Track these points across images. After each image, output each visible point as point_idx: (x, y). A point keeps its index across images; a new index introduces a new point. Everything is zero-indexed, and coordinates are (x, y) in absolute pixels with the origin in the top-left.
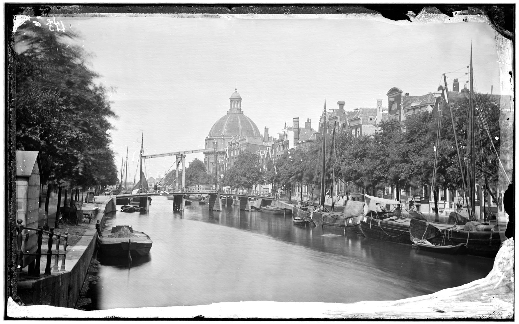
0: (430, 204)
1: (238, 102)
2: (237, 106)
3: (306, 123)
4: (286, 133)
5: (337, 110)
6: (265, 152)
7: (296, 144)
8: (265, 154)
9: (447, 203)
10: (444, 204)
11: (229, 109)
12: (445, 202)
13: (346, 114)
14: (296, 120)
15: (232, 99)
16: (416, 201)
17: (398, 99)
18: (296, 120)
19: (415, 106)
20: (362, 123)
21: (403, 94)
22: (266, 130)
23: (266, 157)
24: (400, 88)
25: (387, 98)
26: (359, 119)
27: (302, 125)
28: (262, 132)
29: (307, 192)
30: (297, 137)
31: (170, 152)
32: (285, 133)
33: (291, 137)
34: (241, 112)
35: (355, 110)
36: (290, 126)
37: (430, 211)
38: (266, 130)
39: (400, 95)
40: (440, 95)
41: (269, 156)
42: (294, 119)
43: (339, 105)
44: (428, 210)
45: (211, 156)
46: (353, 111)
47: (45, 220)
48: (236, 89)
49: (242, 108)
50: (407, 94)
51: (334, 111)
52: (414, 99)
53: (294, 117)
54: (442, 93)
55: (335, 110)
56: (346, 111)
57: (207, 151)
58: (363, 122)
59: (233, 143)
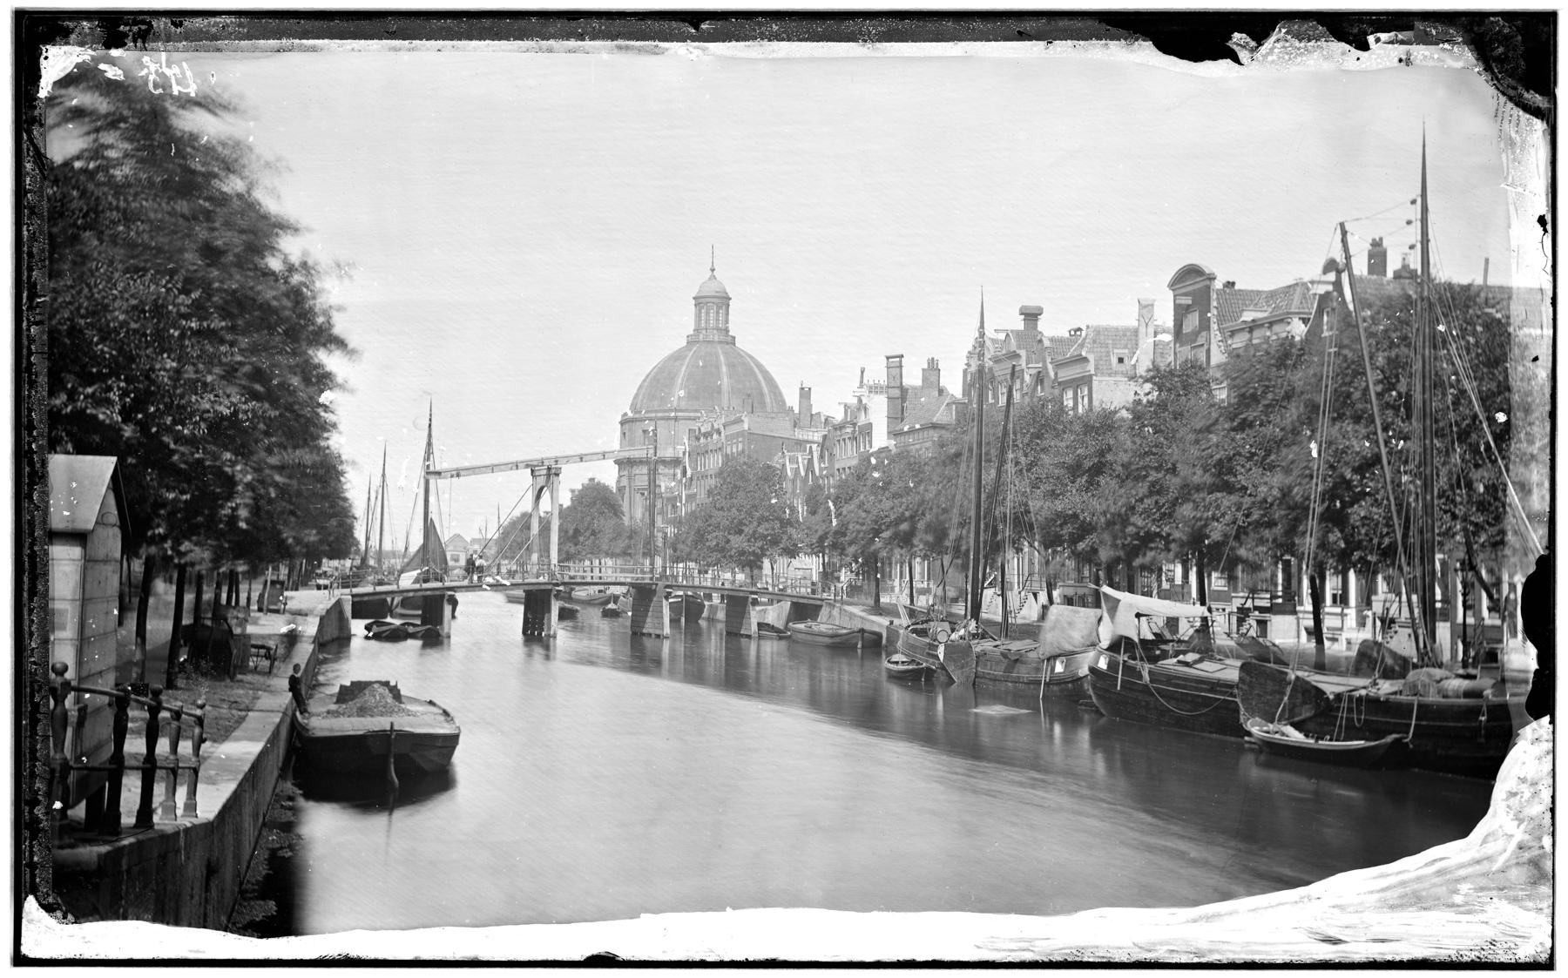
0: (1301, 615)
1: (719, 308)
2: (718, 320)
3: (923, 370)
4: (864, 401)
5: (1018, 333)
6: (800, 460)
7: (894, 434)
8: (801, 465)
9: (1351, 612)
10: (1343, 615)
11: (693, 328)
12: (1346, 611)
13: (1047, 343)
14: (895, 363)
15: (701, 300)
16: (1256, 608)
17: (1201, 299)
18: (895, 363)
19: (1253, 321)
20: (1093, 372)
21: (1218, 284)
22: (805, 394)
23: (803, 474)
24: (1208, 266)
25: (1170, 294)
26: (1085, 358)
27: (913, 377)
28: (792, 400)
29: (929, 579)
30: (897, 413)
31: (514, 460)
32: (860, 401)
33: (878, 413)
34: (729, 339)
35: (1073, 333)
36: (876, 382)
37: (1298, 637)
38: (805, 394)
39: (1208, 287)
40: (1330, 288)
41: (813, 472)
42: (888, 358)
43: (1023, 317)
44: (1294, 633)
45: (637, 472)
46: (1067, 335)
47: (136, 664)
48: (713, 270)
49: (731, 326)
50: (1229, 282)
51: (1008, 335)
52: (1251, 297)
53: (889, 354)
54: (1336, 281)
55: (1012, 331)
56: (1046, 334)
57: (627, 455)
58: (1097, 368)
59: (703, 430)
